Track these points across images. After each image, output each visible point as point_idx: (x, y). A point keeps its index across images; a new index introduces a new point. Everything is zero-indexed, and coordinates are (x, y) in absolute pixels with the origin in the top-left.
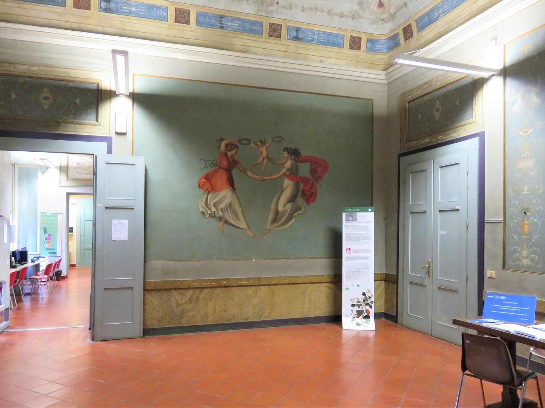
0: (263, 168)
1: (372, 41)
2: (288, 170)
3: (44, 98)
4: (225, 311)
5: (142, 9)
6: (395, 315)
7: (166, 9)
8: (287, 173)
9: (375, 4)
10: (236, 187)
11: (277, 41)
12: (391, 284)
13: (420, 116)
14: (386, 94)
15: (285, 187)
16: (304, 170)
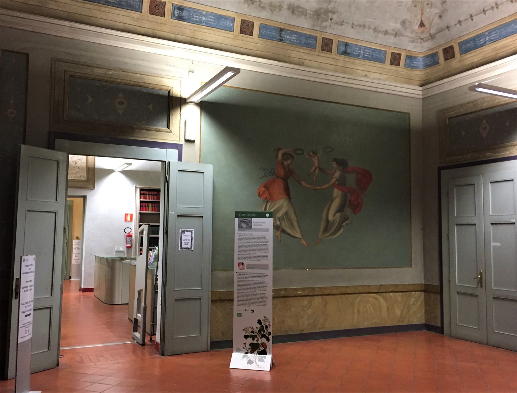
0: (315, 178)
1: (410, 58)
2: (337, 180)
3: (123, 103)
4: (283, 322)
5: (211, 19)
6: (439, 325)
7: (233, 20)
8: (336, 183)
9: (417, 24)
10: (291, 196)
11: (328, 55)
12: (432, 295)
13: (464, 133)
14: (421, 108)
15: (334, 196)
16: (351, 179)
